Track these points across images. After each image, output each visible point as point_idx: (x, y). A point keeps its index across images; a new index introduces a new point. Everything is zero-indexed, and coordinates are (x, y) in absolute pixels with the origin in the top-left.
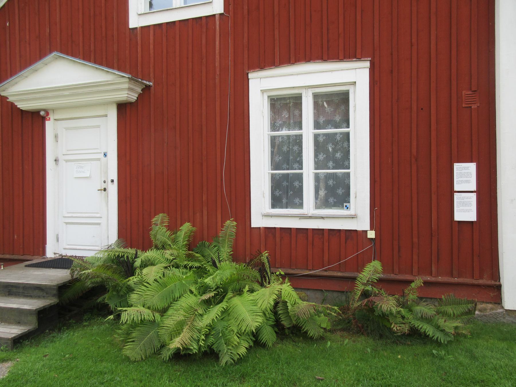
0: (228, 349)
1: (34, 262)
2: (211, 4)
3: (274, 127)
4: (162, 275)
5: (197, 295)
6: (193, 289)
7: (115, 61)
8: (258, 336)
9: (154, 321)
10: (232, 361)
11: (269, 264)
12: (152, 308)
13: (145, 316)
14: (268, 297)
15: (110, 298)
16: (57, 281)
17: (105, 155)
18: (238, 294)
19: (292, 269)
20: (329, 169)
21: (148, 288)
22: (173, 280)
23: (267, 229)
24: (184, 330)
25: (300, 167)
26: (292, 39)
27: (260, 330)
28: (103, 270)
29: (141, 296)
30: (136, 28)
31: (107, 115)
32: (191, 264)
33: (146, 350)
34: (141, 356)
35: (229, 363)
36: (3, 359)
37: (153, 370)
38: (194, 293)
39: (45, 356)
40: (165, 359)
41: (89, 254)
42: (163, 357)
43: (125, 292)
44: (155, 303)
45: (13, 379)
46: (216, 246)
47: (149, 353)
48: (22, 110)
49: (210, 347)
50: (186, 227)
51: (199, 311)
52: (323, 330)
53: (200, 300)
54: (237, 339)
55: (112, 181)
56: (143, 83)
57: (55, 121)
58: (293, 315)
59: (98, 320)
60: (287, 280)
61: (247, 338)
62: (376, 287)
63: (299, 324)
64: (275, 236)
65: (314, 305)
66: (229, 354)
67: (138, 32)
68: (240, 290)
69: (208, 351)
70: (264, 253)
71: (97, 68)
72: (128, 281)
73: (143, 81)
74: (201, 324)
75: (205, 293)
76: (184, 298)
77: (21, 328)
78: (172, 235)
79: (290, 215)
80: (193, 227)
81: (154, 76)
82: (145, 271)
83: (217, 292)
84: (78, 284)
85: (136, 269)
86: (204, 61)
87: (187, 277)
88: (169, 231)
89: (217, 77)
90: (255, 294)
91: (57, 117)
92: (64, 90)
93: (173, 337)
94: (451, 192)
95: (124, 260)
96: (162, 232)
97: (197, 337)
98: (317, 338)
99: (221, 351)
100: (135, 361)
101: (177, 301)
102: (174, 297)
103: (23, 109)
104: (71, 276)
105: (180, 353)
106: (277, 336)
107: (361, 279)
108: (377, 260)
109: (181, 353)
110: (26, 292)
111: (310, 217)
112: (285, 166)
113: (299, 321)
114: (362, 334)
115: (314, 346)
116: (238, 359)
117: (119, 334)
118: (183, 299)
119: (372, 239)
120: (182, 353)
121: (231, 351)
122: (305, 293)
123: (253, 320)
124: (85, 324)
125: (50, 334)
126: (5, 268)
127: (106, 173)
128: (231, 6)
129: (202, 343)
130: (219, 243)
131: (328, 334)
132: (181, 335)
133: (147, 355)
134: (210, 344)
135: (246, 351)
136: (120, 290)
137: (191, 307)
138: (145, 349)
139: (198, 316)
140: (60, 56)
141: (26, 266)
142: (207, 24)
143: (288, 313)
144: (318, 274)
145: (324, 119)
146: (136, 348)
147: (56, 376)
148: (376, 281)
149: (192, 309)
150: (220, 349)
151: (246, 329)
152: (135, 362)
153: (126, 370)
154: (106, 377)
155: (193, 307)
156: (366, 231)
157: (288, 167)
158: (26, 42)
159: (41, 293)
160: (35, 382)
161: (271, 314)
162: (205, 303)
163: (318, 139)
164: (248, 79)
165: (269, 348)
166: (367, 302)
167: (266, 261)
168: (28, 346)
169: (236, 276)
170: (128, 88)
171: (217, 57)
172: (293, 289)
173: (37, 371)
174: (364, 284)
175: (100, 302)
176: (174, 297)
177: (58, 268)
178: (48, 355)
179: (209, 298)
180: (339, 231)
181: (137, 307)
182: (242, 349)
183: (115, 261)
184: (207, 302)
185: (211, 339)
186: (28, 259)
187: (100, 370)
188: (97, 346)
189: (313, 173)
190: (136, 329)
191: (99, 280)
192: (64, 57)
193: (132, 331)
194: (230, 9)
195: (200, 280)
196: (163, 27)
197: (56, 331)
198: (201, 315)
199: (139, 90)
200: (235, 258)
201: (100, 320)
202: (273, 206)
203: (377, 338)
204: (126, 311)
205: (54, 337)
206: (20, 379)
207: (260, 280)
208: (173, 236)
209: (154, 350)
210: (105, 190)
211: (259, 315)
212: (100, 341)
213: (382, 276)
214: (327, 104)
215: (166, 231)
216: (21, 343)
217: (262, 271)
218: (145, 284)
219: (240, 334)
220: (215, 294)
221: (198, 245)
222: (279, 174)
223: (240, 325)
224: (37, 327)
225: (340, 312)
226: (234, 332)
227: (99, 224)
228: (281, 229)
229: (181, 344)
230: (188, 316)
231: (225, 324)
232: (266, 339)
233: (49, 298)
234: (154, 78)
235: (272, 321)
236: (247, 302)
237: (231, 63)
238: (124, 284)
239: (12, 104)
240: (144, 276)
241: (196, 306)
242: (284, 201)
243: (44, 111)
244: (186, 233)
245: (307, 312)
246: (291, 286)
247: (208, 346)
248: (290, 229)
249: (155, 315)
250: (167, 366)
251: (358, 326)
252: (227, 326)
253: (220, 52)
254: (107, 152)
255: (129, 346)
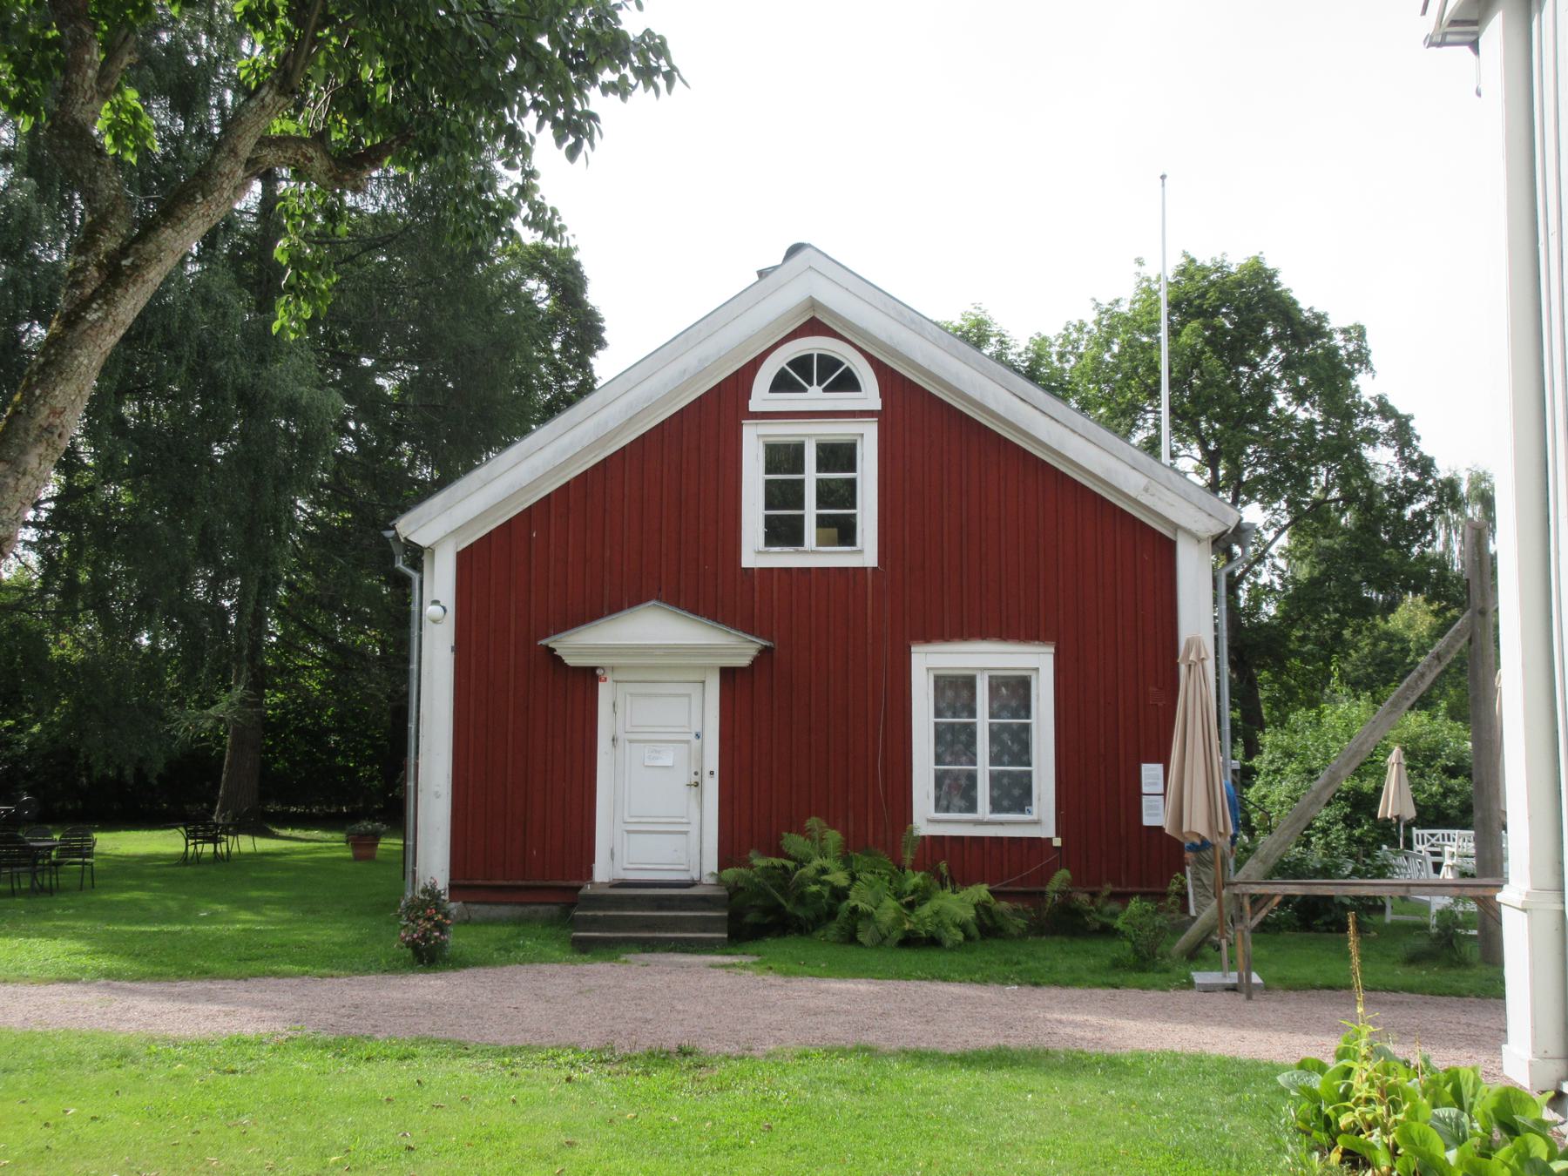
23: (933, 838)
55: (712, 773)
91: (618, 677)
94: (1139, 794)
180: (1021, 839)
210: (696, 785)
227: (686, 833)
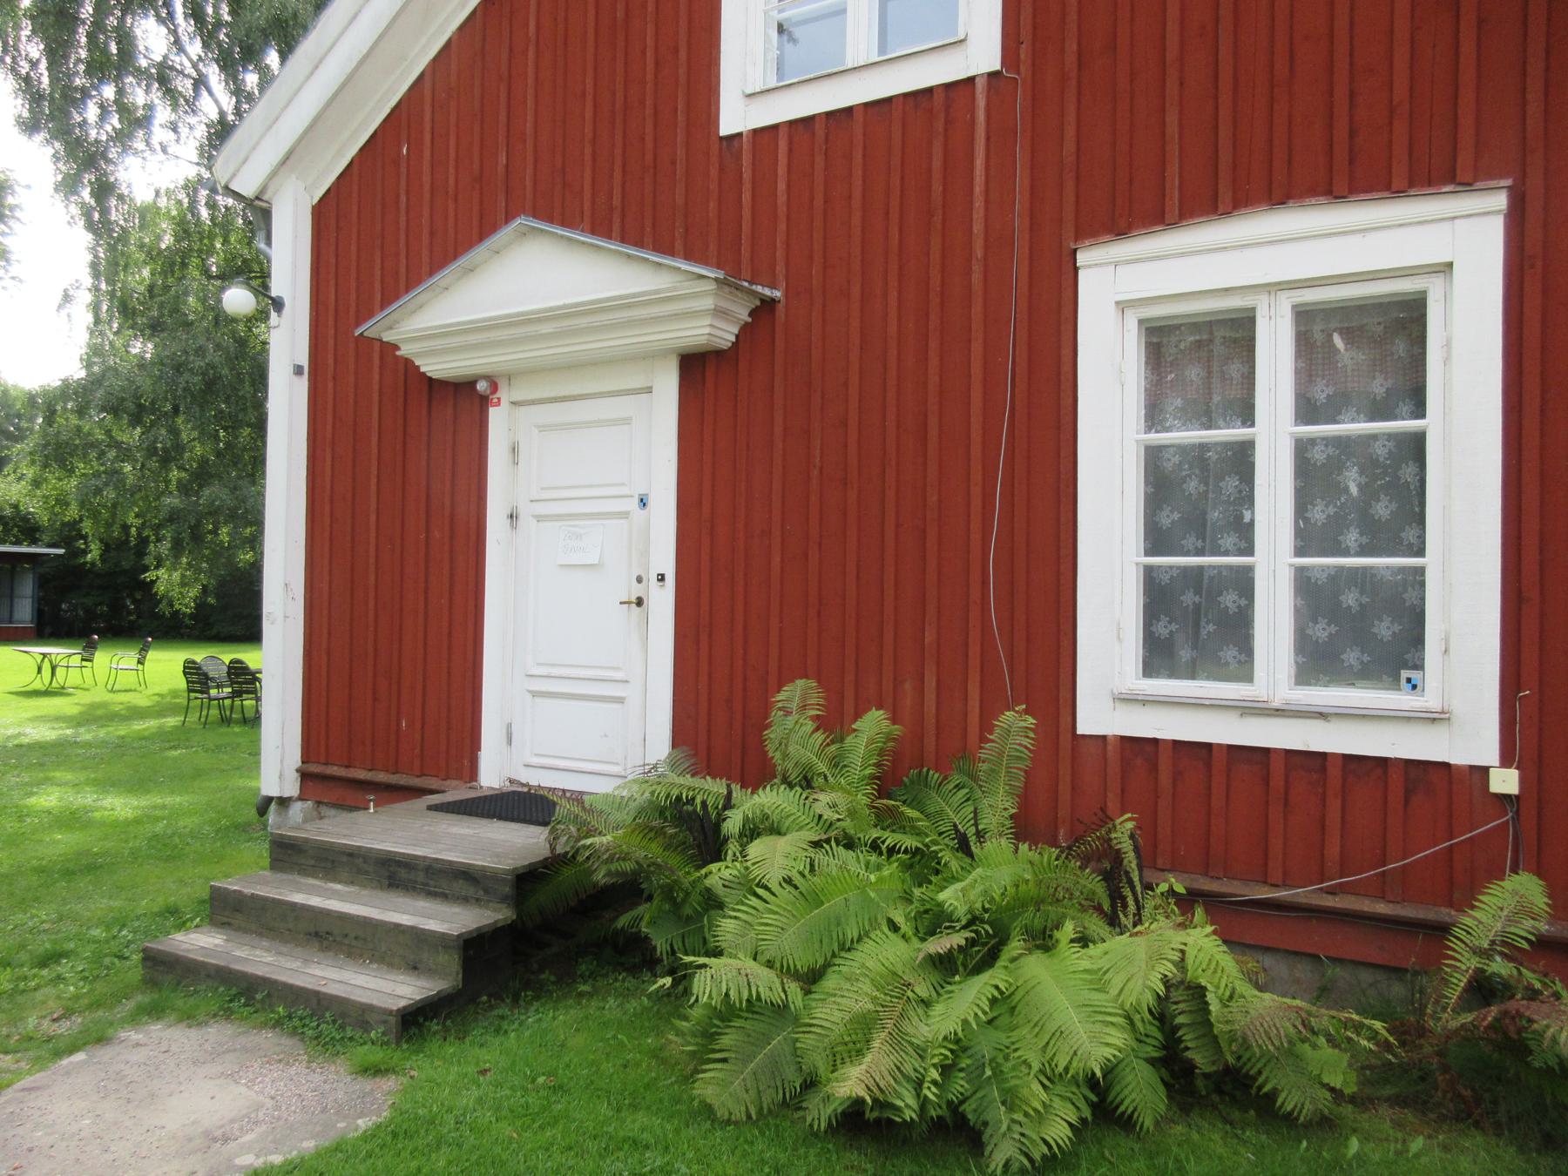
0: (1013, 1121)
1: (450, 797)
2: (963, 46)
3: (1154, 416)
4: (808, 867)
5: (909, 938)
6: (899, 919)
7: (677, 234)
8: (1109, 1088)
9: (786, 1006)
10: (1026, 1162)
11: (1138, 856)
12: (778, 965)
13: (761, 989)
14: (1144, 966)
15: (652, 923)
16: (513, 859)
17: (643, 502)
18: (1038, 947)
19: (1212, 877)
20: (1346, 553)
21: (767, 903)
22: (839, 884)
24: (876, 1044)
25: (1243, 545)
26: (1225, 132)
27: (1116, 1072)
28: (639, 839)
29: (748, 927)
30: (740, 135)
31: (651, 387)
32: (891, 839)
33: (759, 1092)
34: (747, 1107)
35: (1015, 1167)
36: (376, 1066)
37: (783, 1158)
38: (902, 931)
39: (484, 1072)
40: (816, 1127)
41: (599, 787)
42: (809, 1120)
43: (700, 909)
44: (788, 952)
45: (404, 1127)
46: (963, 788)
47: (770, 1100)
48: (430, 379)
49: (953, 1107)
50: (873, 725)
51: (918, 990)
52: (1328, 1095)
53: (921, 956)
54: (1042, 1091)
55: (661, 578)
56: (755, 293)
57: (513, 406)
58: (1226, 1033)
59: (616, 980)
60: (1199, 913)
61: (1074, 1093)
62: (1525, 964)
63: (1245, 1064)
64: (1154, 768)
65: (1301, 1008)
66: (1017, 1136)
67: (745, 147)
68: (1044, 932)
69: (948, 1120)
70: (1122, 819)
71: (629, 256)
72: (706, 876)
73: (754, 287)
74: (924, 1029)
75: (933, 933)
76: (871, 942)
77: (419, 983)
78: (828, 745)
79: (1207, 702)
80: (894, 724)
81: (787, 270)
82: (756, 849)
83: (973, 935)
84: (567, 872)
85: (726, 840)
86: (937, 219)
87: (880, 880)
88: (821, 731)
89: (977, 268)
90: (1093, 950)
91: (518, 395)
92: (539, 320)
93: (838, 1062)
95: (695, 810)
96: (800, 734)
97: (915, 1070)
98: (1311, 1120)
99: (991, 1124)
100: (729, 1120)
101: (849, 950)
102: (841, 937)
103: (435, 375)
104: (548, 846)
105: (864, 1113)
106: (1170, 1097)
107: (1468, 933)
108: (1530, 871)
109: (867, 1115)
110: (432, 883)
111: (1279, 713)
112: (1190, 541)
113: (1246, 1056)
114: (1477, 1125)
115: (1298, 1148)
116: (1044, 1156)
117: (679, 1033)
118: (868, 946)
119: (1507, 797)
120: (870, 1115)
121: (1020, 1130)
122: (1258, 962)
123: (1094, 1037)
124: (583, 988)
125: (491, 1008)
126: (379, 809)
127: (645, 553)
128: (1023, 46)
129: (930, 1093)
130: (974, 778)
131: (1347, 1110)
132: (866, 1060)
133: (762, 1108)
134: (954, 1099)
135: (1071, 1135)
136: (684, 901)
137: (895, 974)
138: (758, 1088)
139: (914, 1003)
140: (534, 228)
141: (430, 808)
142: (947, 108)
143: (1210, 1025)
144: (1304, 901)
145: (1330, 390)
146: (732, 1083)
147: (515, 1135)
148: (1525, 945)
149: (899, 979)
150: (988, 1116)
151: (1070, 1062)
152: (729, 1122)
153: (705, 1145)
154: (649, 1158)
155: (900, 973)
156: (1484, 771)
157: (1199, 544)
158: (447, 193)
159: (470, 891)
160: (460, 1146)
161: (1151, 1023)
162: (934, 964)
163: (1309, 455)
164: (1076, 270)
165: (1143, 1134)
166: (1496, 1019)
167: (1126, 846)
168: (438, 1037)
169: (1032, 890)
170: (715, 310)
171: (977, 205)
172: (1224, 948)
173: (464, 1115)
174: (1478, 952)
175: (623, 927)
176: (841, 937)
177: (513, 820)
178: (489, 1070)
179: (950, 950)
180: (1205, 750)
181: (736, 957)
182: (1057, 1125)
183: (668, 814)
184: (941, 963)
185: (960, 1084)
186: (433, 787)
187: (631, 1134)
188: (620, 1062)
189: (1291, 565)
190: (732, 1024)
191: (628, 866)
192: (542, 230)
193: (718, 1027)
194: (1022, 56)
195: (920, 890)
196: (817, 126)
197: (508, 1001)
198: (922, 1000)
199: (744, 316)
200: (1024, 829)
201: (623, 981)
202: (1149, 670)
203: (1532, 1145)
204: (704, 966)
205: (502, 1018)
206: (422, 1132)
207: (1106, 906)
208: (833, 748)
209: (784, 1094)
211: (1112, 1023)
212: (626, 1046)
213: (1543, 927)
214: (1343, 339)
215: (813, 732)
216: (420, 1026)
217: (1113, 875)
218: (760, 891)
219: (1050, 1078)
220: (966, 939)
221: (905, 778)
222: (1171, 567)
223: (1048, 1051)
224: (460, 986)
225: (1391, 1039)
226: (1030, 1067)
227: (620, 700)
228: (1177, 744)
229: (867, 1086)
230: (885, 1001)
231: (1002, 1038)
232: (1134, 1104)
233: (491, 904)
234: (787, 278)
235: (1154, 1046)
236: (1071, 976)
237: (1019, 223)
238: (694, 884)
239: (408, 363)
240: (754, 864)
241: (907, 970)
242: (1185, 654)
243: (487, 381)
244: (871, 741)
245: (1277, 1029)
246: (1215, 937)
247: (950, 1103)
248: (1208, 746)
249: (786, 988)
250: (822, 1149)
251: (1460, 1095)
252: (1007, 1048)
253: (987, 192)
254: (647, 495)
255: (712, 1073)
